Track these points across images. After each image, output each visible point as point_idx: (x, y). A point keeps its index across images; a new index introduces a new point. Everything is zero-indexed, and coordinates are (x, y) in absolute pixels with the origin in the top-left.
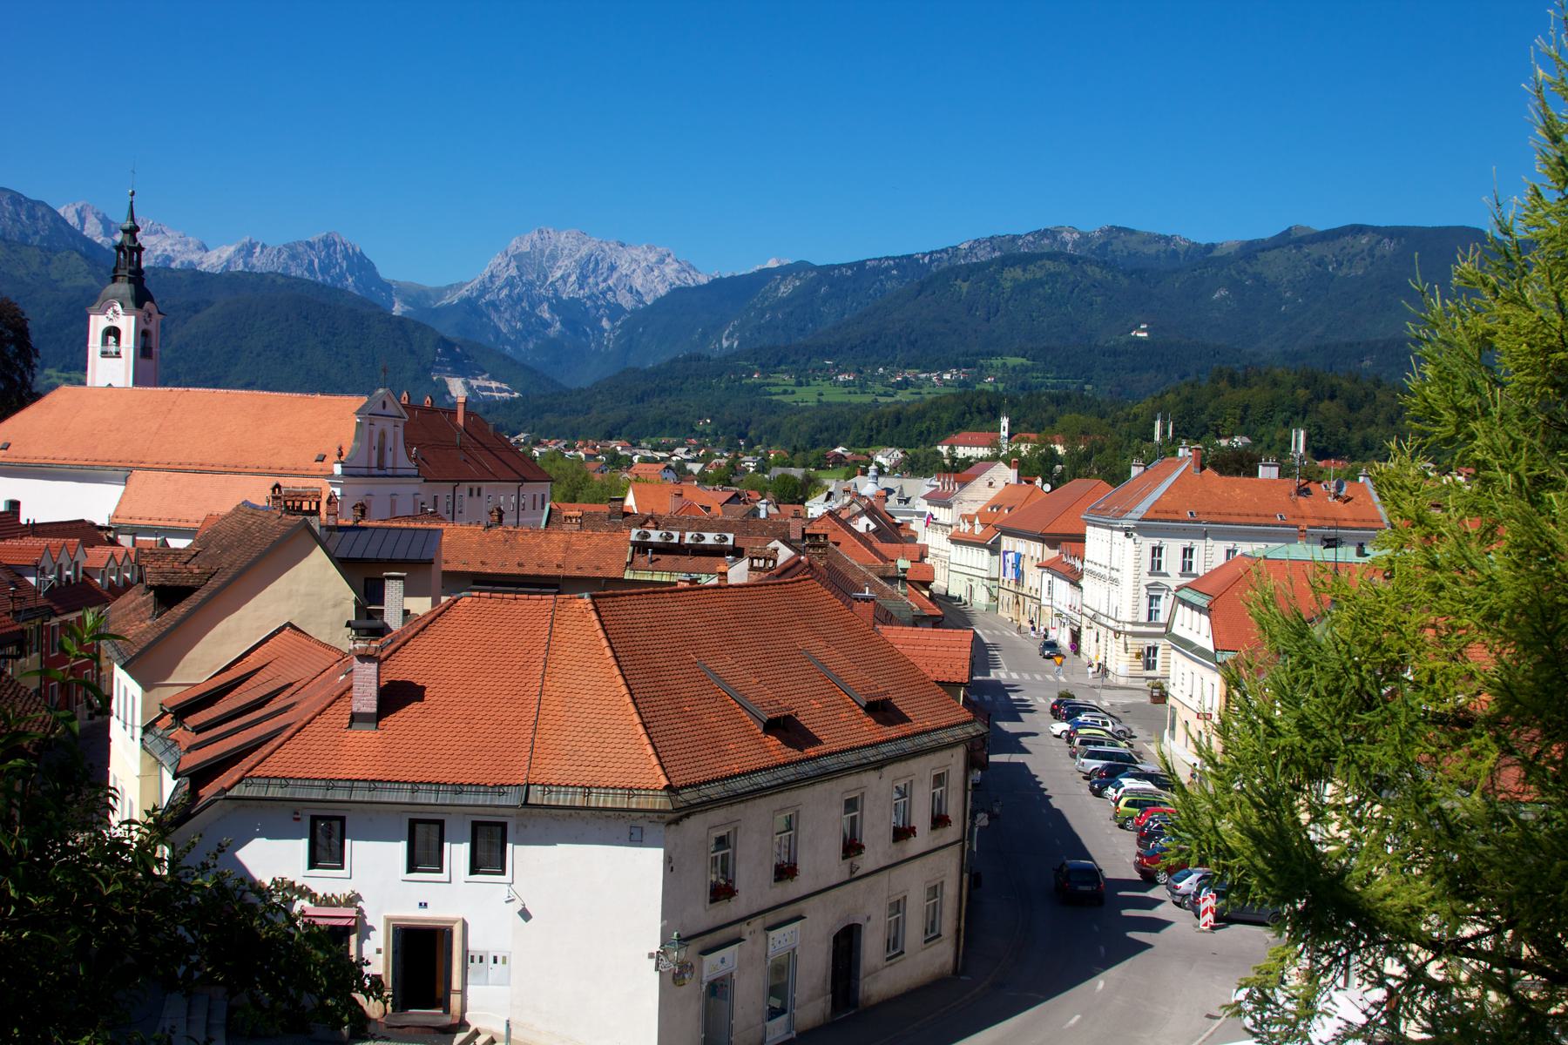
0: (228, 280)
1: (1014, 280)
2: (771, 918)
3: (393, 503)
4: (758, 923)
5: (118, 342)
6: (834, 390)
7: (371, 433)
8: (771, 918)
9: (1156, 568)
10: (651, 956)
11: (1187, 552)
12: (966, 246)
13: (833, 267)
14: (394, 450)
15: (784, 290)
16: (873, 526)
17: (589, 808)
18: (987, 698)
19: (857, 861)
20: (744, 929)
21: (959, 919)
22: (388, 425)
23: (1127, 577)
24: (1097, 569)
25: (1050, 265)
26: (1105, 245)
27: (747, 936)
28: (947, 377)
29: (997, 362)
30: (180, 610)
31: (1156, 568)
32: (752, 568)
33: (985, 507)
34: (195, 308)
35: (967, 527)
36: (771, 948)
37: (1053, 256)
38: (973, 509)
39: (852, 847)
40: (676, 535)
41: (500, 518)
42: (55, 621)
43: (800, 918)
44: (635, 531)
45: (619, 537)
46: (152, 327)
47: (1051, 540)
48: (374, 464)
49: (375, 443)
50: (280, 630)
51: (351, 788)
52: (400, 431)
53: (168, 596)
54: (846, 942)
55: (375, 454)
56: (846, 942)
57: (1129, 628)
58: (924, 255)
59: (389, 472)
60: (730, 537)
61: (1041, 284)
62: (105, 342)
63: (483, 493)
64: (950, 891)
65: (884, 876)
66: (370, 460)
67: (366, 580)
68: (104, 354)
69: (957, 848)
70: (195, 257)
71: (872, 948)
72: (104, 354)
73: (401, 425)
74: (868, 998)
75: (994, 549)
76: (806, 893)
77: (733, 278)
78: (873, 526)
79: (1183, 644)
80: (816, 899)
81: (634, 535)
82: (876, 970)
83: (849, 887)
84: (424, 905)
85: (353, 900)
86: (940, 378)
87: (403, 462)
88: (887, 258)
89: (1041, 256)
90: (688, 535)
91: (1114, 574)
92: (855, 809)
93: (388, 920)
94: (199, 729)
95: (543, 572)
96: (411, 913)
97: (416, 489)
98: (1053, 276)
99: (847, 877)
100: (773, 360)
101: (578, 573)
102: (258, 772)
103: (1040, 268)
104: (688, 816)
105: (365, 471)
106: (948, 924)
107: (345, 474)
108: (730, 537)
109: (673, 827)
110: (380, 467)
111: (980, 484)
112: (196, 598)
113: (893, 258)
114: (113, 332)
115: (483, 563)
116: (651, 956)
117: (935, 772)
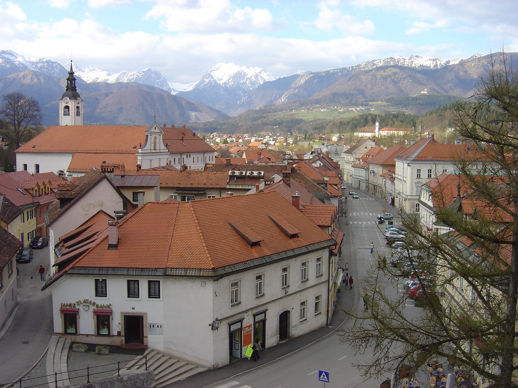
4: (250, 313)
5: (69, 110)
6: (322, 113)
9: (419, 176)
10: (210, 325)
11: (430, 171)
14: (159, 143)
16: (322, 164)
17: (186, 276)
18: (356, 223)
22: (158, 136)
23: (408, 180)
24: (399, 177)
25: (395, 70)
28: (358, 109)
31: (419, 176)
32: (266, 184)
33: (364, 155)
34: (107, 95)
35: (358, 162)
38: (360, 156)
39: (305, 279)
40: (244, 172)
44: (230, 171)
45: (225, 174)
46: (79, 105)
47: (384, 165)
51: (108, 270)
52: (161, 137)
54: (284, 317)
55: (153, 145)
56: (284, 317)
57: (409, 197)
59: (158, 151)
60: (262, 173)
61: (390, 76)
63: (191, 156)
64: (324, 298)
68: (64, 115)
69: (327, 284)
71: (294, 318)
72: (64, 115)
73: (162, 135)
74: (293, 335)
75: (367, 169)
78: (322, 164)
79: (425, 204)
80: (273, 304)
81: (230, 173)
82: (296, 326)
83: (285, 299)
84: (133, 308)
85: (108, 306)
87: (163, 147)
90: (248, 172)
91: (405, 179)
93: (122, 313)
94: (69, 247)
95: (200, 186)
96: (129, 310)
97: (167, 156)
98: (395, 73)
100: (303, 103)
101: (211, 186)
102: (77, 265)
105: (149, 151)
106: (323, 308)
108: (262, 173)
113: (339, 69)
114: (67, 107)
116: (210, 325)
117: (284, 267)
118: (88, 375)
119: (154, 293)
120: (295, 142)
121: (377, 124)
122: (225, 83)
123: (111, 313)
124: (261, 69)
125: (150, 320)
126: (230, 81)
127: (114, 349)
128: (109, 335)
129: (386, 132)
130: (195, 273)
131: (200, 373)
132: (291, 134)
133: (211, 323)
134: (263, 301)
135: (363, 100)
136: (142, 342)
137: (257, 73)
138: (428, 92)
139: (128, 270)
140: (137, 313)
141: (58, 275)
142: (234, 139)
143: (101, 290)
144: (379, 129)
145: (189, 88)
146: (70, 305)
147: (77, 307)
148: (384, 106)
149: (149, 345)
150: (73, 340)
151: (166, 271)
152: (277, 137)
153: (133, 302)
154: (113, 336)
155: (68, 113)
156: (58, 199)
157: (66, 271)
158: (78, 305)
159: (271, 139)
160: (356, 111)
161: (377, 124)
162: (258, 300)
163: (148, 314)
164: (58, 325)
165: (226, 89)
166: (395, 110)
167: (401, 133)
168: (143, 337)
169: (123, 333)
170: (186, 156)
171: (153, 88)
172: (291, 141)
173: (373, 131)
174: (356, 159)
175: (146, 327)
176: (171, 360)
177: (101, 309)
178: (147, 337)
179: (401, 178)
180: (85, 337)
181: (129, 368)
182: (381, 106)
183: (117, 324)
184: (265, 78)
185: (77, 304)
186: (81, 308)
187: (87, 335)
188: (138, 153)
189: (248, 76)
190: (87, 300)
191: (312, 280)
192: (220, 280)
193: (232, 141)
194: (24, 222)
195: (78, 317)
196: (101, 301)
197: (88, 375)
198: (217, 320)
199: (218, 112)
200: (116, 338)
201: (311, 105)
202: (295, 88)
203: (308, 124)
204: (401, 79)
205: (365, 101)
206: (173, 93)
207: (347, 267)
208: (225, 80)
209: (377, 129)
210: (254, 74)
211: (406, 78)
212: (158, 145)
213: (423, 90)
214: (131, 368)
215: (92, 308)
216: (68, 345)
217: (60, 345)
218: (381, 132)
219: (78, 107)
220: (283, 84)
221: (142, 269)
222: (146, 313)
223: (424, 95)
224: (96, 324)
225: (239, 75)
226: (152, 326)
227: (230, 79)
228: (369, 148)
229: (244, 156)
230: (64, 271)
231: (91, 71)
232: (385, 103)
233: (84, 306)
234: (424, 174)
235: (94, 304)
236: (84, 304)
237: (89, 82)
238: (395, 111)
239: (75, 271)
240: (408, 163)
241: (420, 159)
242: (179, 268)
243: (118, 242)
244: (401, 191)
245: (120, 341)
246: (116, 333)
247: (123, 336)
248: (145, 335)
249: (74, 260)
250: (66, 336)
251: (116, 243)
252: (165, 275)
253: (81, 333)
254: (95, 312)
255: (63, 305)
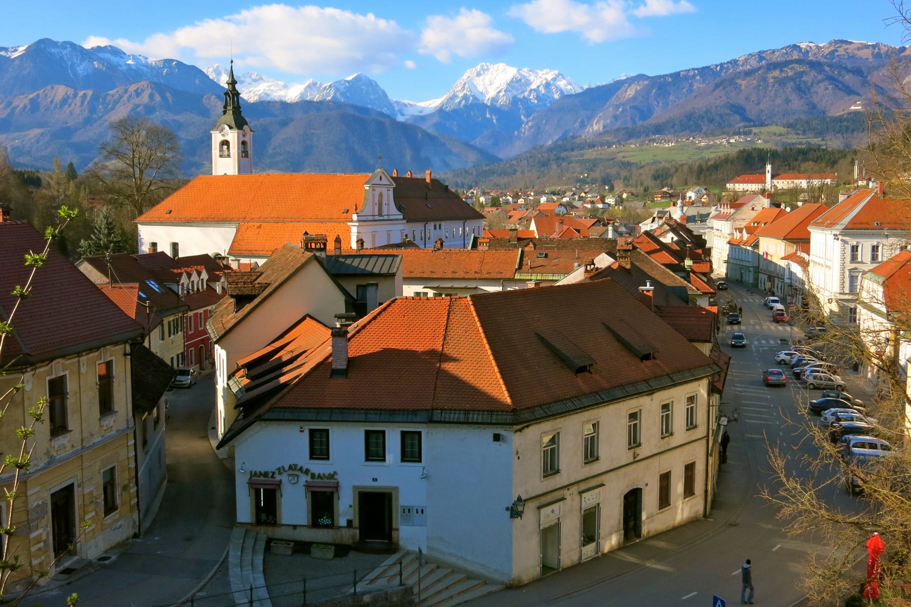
0: (305, 105)
1: (774, 78)
2: (583, 486)
3: (389, 235)
4: (575, 489)
5: (228, 148)
6: (666, 149)
7: (373, 195)
8: (583, 486)
10: (507, 509)
11: (875, 249)
12: (743, 58)
13: (660, 77)
15: (631, 92)
19: (638, 450)
20: (566, 493)
21: (706, 485)
22: (384, 191)
25: (799, 68)
26: (833, 52)
27: (568, 497)
28: (732, 141)
29: (764, 130)
30: (248, 307)
33: (750, 223)
34: (284, 124)
36: (583, 503)
37: (799, 62)
39: (634, 441)
41: (442, 244)
42: (191, 314)
43: (602, 485)
46: (247, 139)
48: (377, 213)
49: (377, 201)
50: (303, 319)
53: (241, 300)
54: (632, 501)
55: (377, 208)
56: (632, 501)
58: (717, 66)
59: (386, 218)
62: (221, 150)
63: (443, 227)
65: (656, 459)
66: (373, 211)
67: (358, 286)
68: (221, 156)
69: (704, 441)
70: (282, 93)
71: (650, 500)
72: (221, 156)
73: (392, 190)
76: (541, 492)
77: (598, 88)
78: (676, 238)
80: (612, 474)
84: (375, 480)
85: (331, 476)
86: (729, 143)
87: (394, 210)
88: (693, 69)
89: (792, 62)
91: (828, 263)
92: (636, 419)
93: (355, 488)
96: (367, 483)
97: (401, 227)
98: (802, 74)
99: (632, 460)
102: (279, 404)
103: (791, 69)
104: (527, 426)
105: (371, 218)
107: (359, 221)
109: (518, 433)
110: (380, 215)
111: (746, 209)
112: (256, 301)
113: (697, 69)
114: (225, 143)
115: (432, 272)
116: (507, 509)
118: (305, 592)
119: (411, 451)
120: (620, 201)
121: (769, 167)
122: (494, 100)
123: (337, 487)
124: (556, 72)
125: (403, 500)
126: (501, 94)
127: (342, 550)
128: (331, 526)
129: (786, 182)
130: (482, 418)
131: (490, 593)
132: (612, 189)
133: (510, 506)
134: (596, 468)
135: (742, 124)
136: (390, 537)
137: (549, 79)
138: (863, 105)
139: (366, 414)
140: (381, 488)
141: (242, 423)
142: (511, 199)
143: (319, 447)
144: (773, 177)
145: (431, 104)
146: (266, 474)
147: (278, 477)
148: (780, 135)
149: (401, 543)
150: (270, 535)
151: (432, 414)
152: (585, 193)
153: (374, 468)
154: (339, 527)
155: (226, 153)
156: (232, 296)
157: (260, 416)
158: (280, 473)
159: (577, 197)
160: (730, 144)
161: (769, 167)
162: (588, 467)
163: (401, 490)
164: (245, 511)
165: (494, 108)
166: (804, 141)
167: (816, 182)
168: (391, 529)
169: (356, 523)
170: (433, 227)
171: (366, 111)
172: (610, 200)
173: (764, 181)
174: (736, 229)
175: (397, 510)
176: (440, 570)
177: (319, 480)
178: (397, 530)
179: (822, 261)
180: (291, 529)
181: (372, 581)
182: (775, 134)
183: (346, 507)
184: (563, 87)
185: (277, 472)
186: (284, 478)
187: (295, 527)
188: (352, 221)
189: (533, 86)
190: (296, 465)
191: (680, 433)
192: (526, 430)
193: (507, 202)
194: (163, 339)
195: (278, 495)
196: (319, 467)
197: (305, 592)
198: (519, 499)
199: (480, 151)
200: (344, 530)
201: (647, 135)
202: (618, 107)
203: (641, 171)
204: (812, 84)
205: (746, 127)
206: (400, 119)
207: (736, 416)
208: (491, 93)
209: (768, 176)
210: (544, 82)
211: (823, 81)
212: (385, 208)
213: (854, 103)
214: (381, 577)
215: (304, 479)
216: (261, 546)
217: (250, 543)
218: (775, 181)
219: (244, 143)
220: (596, 98)
221: (392, 412)
222: (396, 489)
223: (856, 113)
224: (310, 507)
225: (517, 83)
226: (407, 511)
227: (499, 92)
228: (759, 208)
229: (533, 227)
230: (256, 414)
231: (255, 81)
232: (782, 130)
233: (289, 475)
234: (865, 253)
235: (307, 472)
236: (291, 472)
237: (252, 101)
238: (800, 143)
239: (271, 416)
240: (835, 235)
241: (857, 228)
242: (450, 410)
243: (348, 366)
244: (822, 285)
245: (350, 536)
246: (343, 522)
247: (355, 528)
248: (394, 526)
249: (272, 397)
250: (258, 528)
251: (345, 367)
252: (431, 421)
253: (284, 522)
254: (308, 486)
255: (254, 474)
